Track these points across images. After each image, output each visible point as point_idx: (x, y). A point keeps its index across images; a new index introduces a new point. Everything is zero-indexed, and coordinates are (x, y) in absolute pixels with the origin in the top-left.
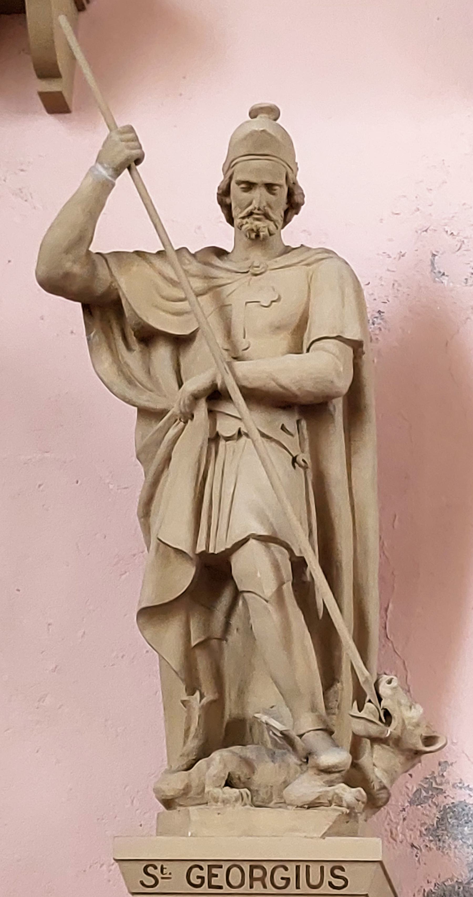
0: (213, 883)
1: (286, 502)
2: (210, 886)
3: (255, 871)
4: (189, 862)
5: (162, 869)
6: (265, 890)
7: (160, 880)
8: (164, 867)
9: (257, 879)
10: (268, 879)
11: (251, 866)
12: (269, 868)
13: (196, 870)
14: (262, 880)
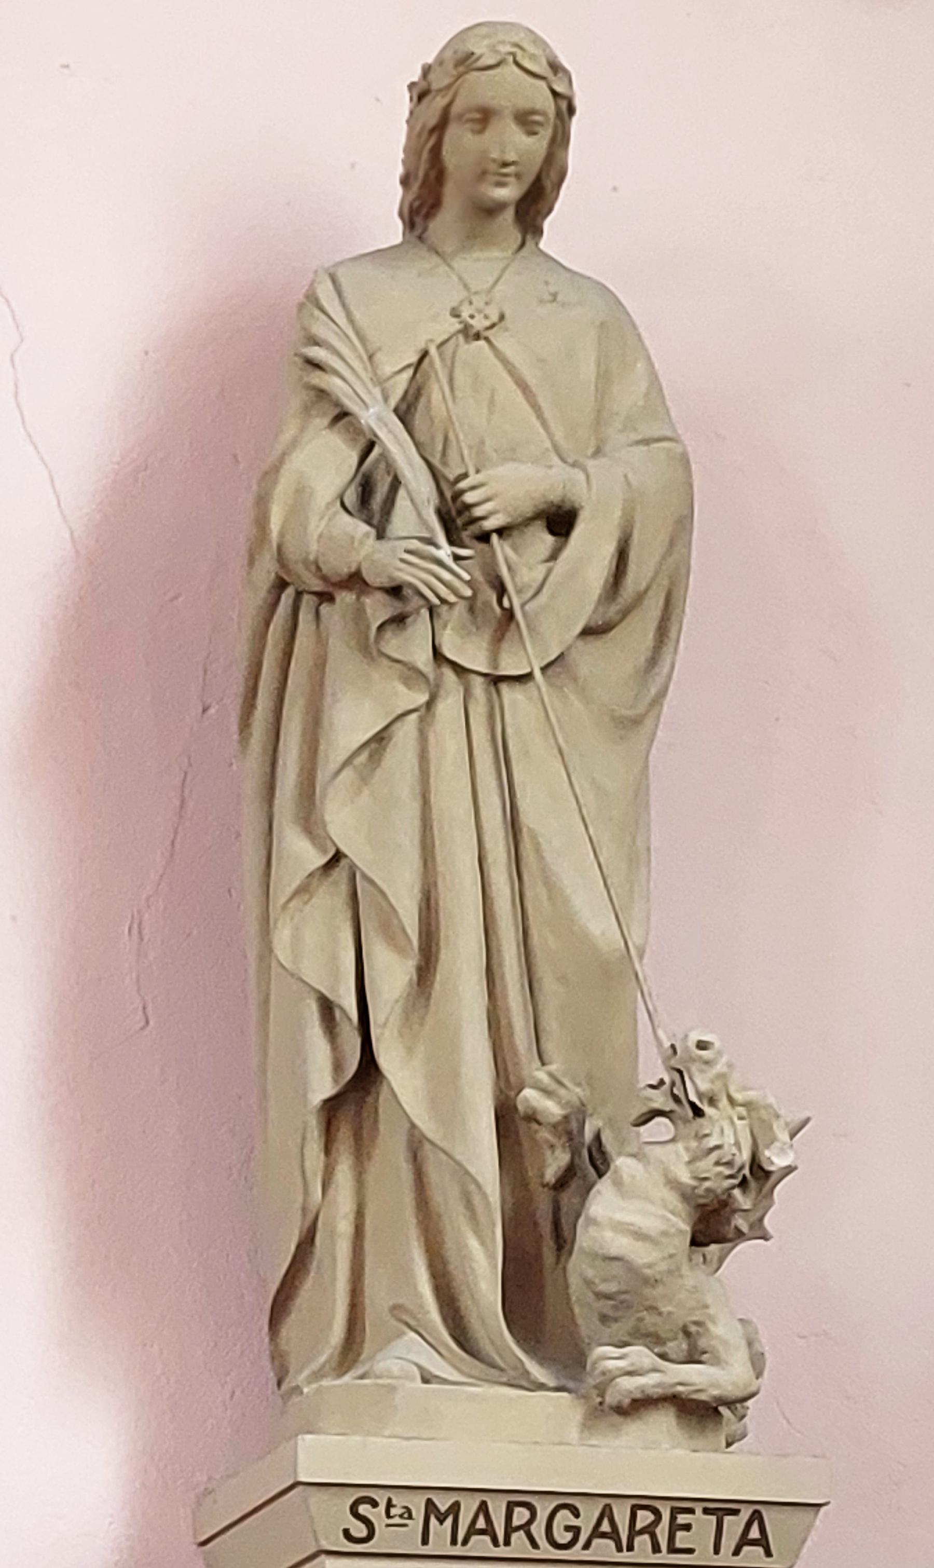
0: (678, 1545)
3: (640, 1513)
4: (477, 1494)
5: (390, 1505)
8: (394, 1502)
10: (538, 1529)
12: (543, 1509)
13: (564, 1515)
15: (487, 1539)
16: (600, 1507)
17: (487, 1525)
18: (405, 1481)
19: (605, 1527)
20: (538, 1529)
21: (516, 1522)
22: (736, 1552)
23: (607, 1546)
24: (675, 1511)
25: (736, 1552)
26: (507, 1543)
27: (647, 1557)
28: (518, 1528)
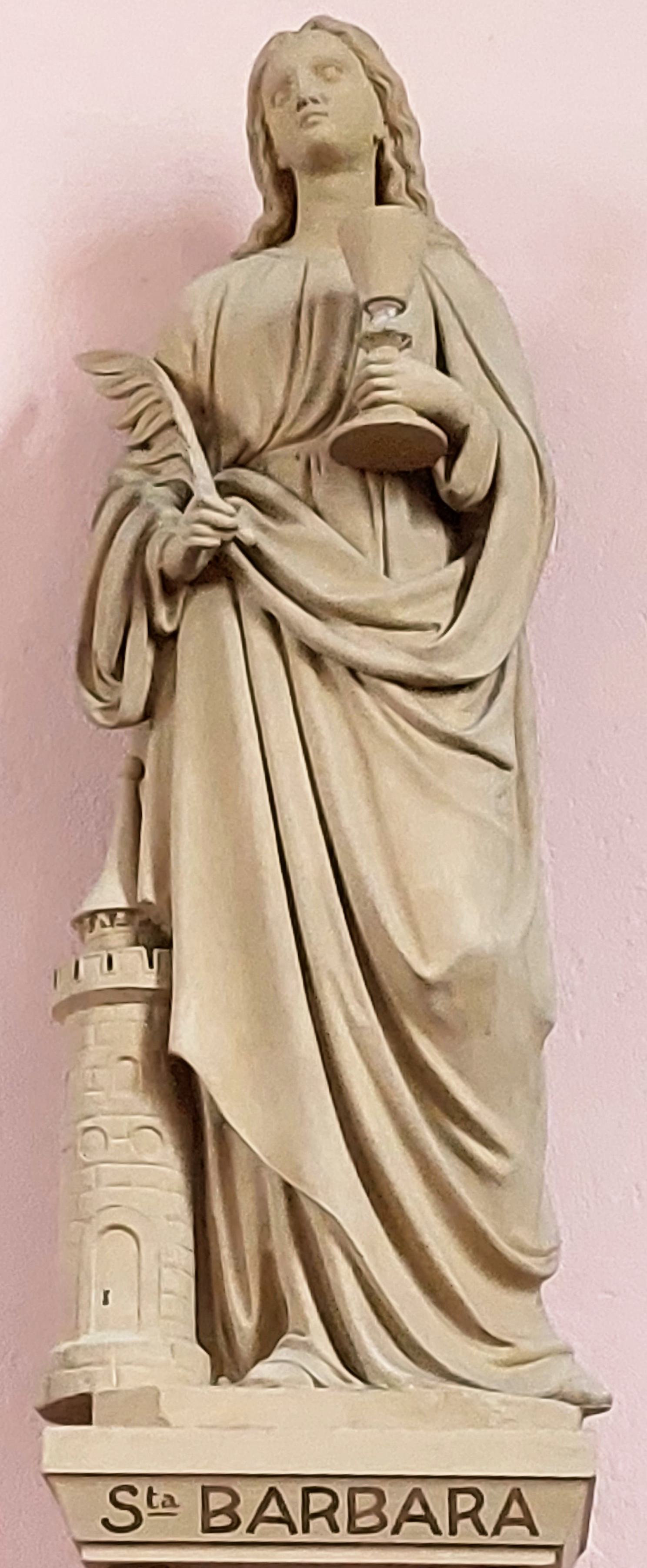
1: (226, 1355)
2: (352, 1529)
3: (212, 1496)
4: (411, 1481)
6: (336, 1535)
7: (144, 1515)
8: (155, 1491)
9: (465, 1515)
10: (341, 1516)
11: (203, 1488)
14: (328, 1514)
15: (426, 1526)
16: (266, 1490)
17: (524, 1514)
18: (65, 1467)
19: (515, 1511)
20: (341, 1516)
21: (460, 1509)
22: (497, 1531)
23: (524, 1532)
24: (273, 1492)
25: (497, 1531)
26: (306, 1530)
27: (198, 1536)
28: (465, 1515)
